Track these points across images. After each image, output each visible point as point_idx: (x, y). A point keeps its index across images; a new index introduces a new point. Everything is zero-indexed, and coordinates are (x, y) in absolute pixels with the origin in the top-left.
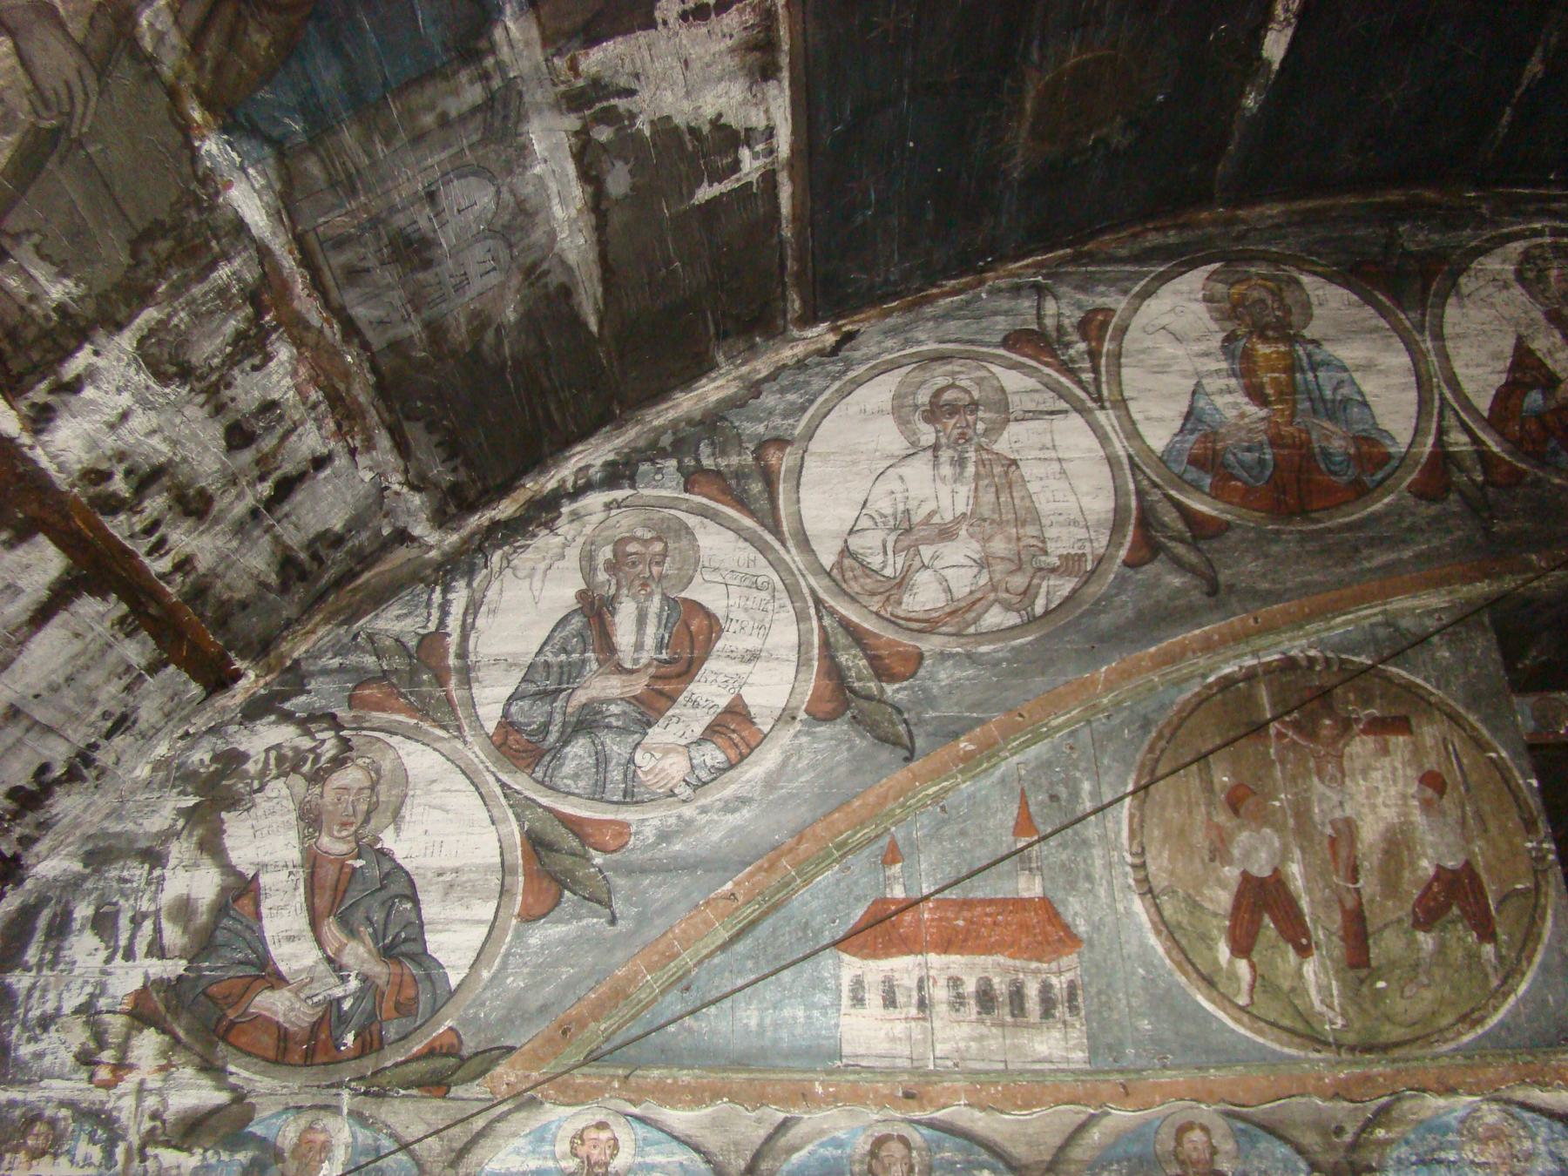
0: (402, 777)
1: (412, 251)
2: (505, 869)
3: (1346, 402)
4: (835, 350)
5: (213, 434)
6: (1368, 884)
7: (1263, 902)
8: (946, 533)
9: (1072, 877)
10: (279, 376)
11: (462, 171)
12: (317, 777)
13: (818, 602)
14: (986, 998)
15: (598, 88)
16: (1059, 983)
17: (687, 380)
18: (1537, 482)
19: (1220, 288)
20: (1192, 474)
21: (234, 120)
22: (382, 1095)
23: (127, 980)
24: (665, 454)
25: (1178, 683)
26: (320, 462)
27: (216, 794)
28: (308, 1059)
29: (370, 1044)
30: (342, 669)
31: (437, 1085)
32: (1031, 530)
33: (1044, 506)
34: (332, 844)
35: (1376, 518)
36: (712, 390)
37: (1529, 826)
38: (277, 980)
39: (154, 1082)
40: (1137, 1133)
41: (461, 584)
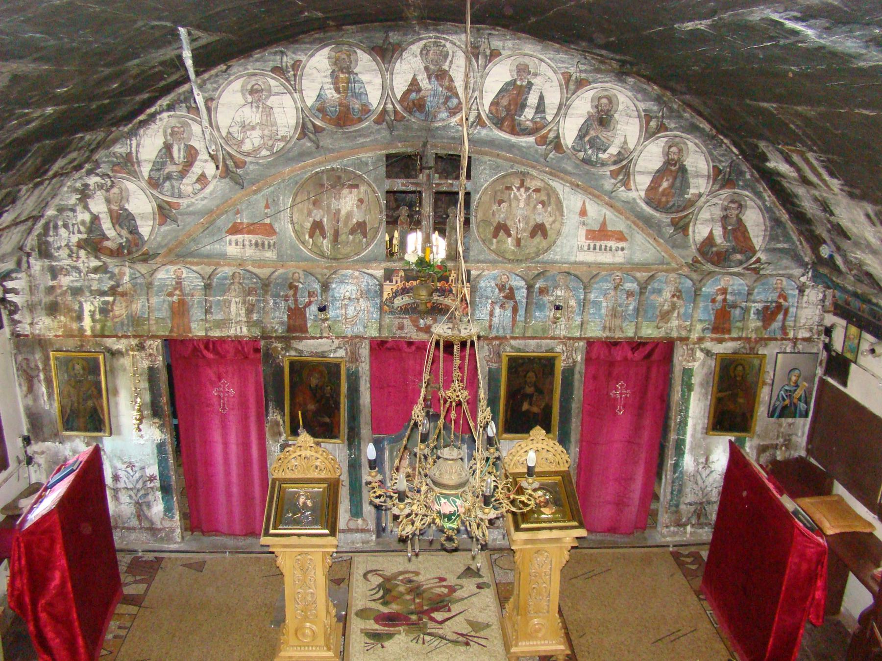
2: (154, 214)
3: (361, 94)
4: (226, 71)
7: (317, 226)
12: (108, 190)
13: (222, 147)
14: (257, 244)
18: (408, 121)
19: (333, 54)
20: (317, 113)
22: (134, 263)
23: (75, 239)
24: (182, 102)
25: (305, 173)
27: (85, 194)
29: (129, 253)
30: (108, 162)
31: (145, 261)
32: (275, 128)
33: (279, 121)
34: (114, 207)
35: (362, 129)
37: (381, 212)
38: (108, 239)
39: (86, 261)
40: (284, 273)
41: (134, 139)
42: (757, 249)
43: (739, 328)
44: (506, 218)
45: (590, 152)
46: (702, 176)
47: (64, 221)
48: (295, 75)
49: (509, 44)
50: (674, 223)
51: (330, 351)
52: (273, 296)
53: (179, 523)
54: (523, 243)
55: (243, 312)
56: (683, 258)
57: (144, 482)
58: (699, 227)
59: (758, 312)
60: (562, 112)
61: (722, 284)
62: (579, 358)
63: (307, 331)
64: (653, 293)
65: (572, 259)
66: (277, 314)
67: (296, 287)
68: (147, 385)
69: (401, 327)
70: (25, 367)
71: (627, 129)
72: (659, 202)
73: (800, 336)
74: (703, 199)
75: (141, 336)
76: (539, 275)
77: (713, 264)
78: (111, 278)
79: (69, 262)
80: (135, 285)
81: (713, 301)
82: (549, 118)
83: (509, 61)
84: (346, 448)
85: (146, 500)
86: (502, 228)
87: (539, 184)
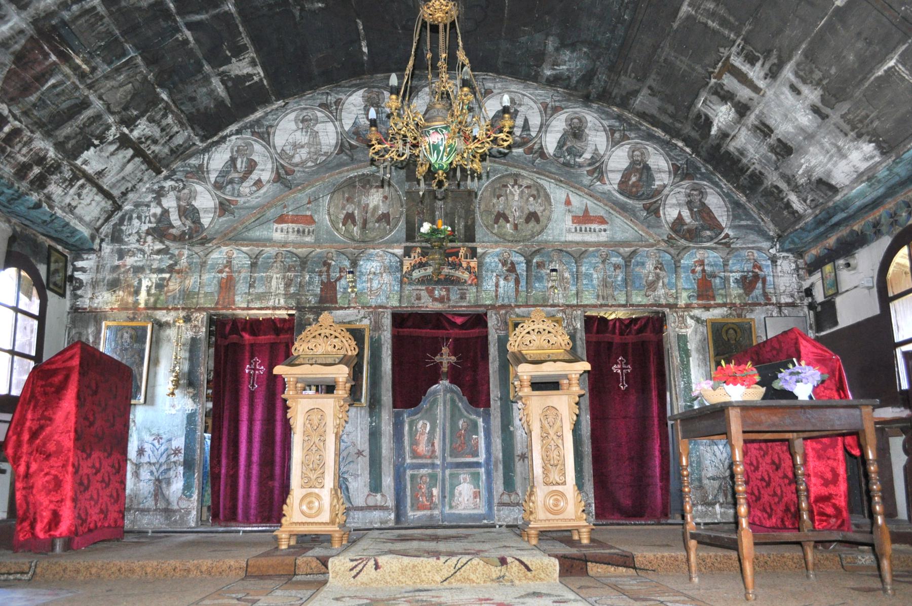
0: (196, 192)
1: (192, 99)
2: (215, 208)
5: (158, 130)
7: (350, 217)
8: (302, 147)
10: (170, 119)
12: (179, 191)
14: (298, 231)
15: (223, 72)
17: (253, 113)
23: (145, 227)
26: (177, 132)
27: (160, 194)
28: (180, 240)
31: (203, 244)
33: (322, 142)
34: (183, 203)
36: (258, 114)
37: (402, 206)
38: (173, 227)
40: (320, 253)
42: (724, 226)
43: (722, 295)
46: (664, 172)
48: (337, 109)
49: (499, 85)
50: (646, 208)
51: (356, 321)
53: (196, 504)
55: (282, 286)
57: (168, 456)
58: (668, 210)
59: (737, 281)
60: (543, 129)
61: (698, 256)
63: (337, 303)
65: (563, 239)
66: (311, 287)
67: (330, 264)
68: (187, 355)
69: (419, 298)
71: (597, 140)
72: (631, 192)
73: (783, 301)
74: (668, 189)
75: (189, 309)
76: (535, 252)
77: (686, 239)
78: (170, 258)
79: (137, 245)
80: (190, 264)
81: (693, 271)
82: (533, 134)
84: (368, 415)
86: (502, 216)
87: (529, 182)
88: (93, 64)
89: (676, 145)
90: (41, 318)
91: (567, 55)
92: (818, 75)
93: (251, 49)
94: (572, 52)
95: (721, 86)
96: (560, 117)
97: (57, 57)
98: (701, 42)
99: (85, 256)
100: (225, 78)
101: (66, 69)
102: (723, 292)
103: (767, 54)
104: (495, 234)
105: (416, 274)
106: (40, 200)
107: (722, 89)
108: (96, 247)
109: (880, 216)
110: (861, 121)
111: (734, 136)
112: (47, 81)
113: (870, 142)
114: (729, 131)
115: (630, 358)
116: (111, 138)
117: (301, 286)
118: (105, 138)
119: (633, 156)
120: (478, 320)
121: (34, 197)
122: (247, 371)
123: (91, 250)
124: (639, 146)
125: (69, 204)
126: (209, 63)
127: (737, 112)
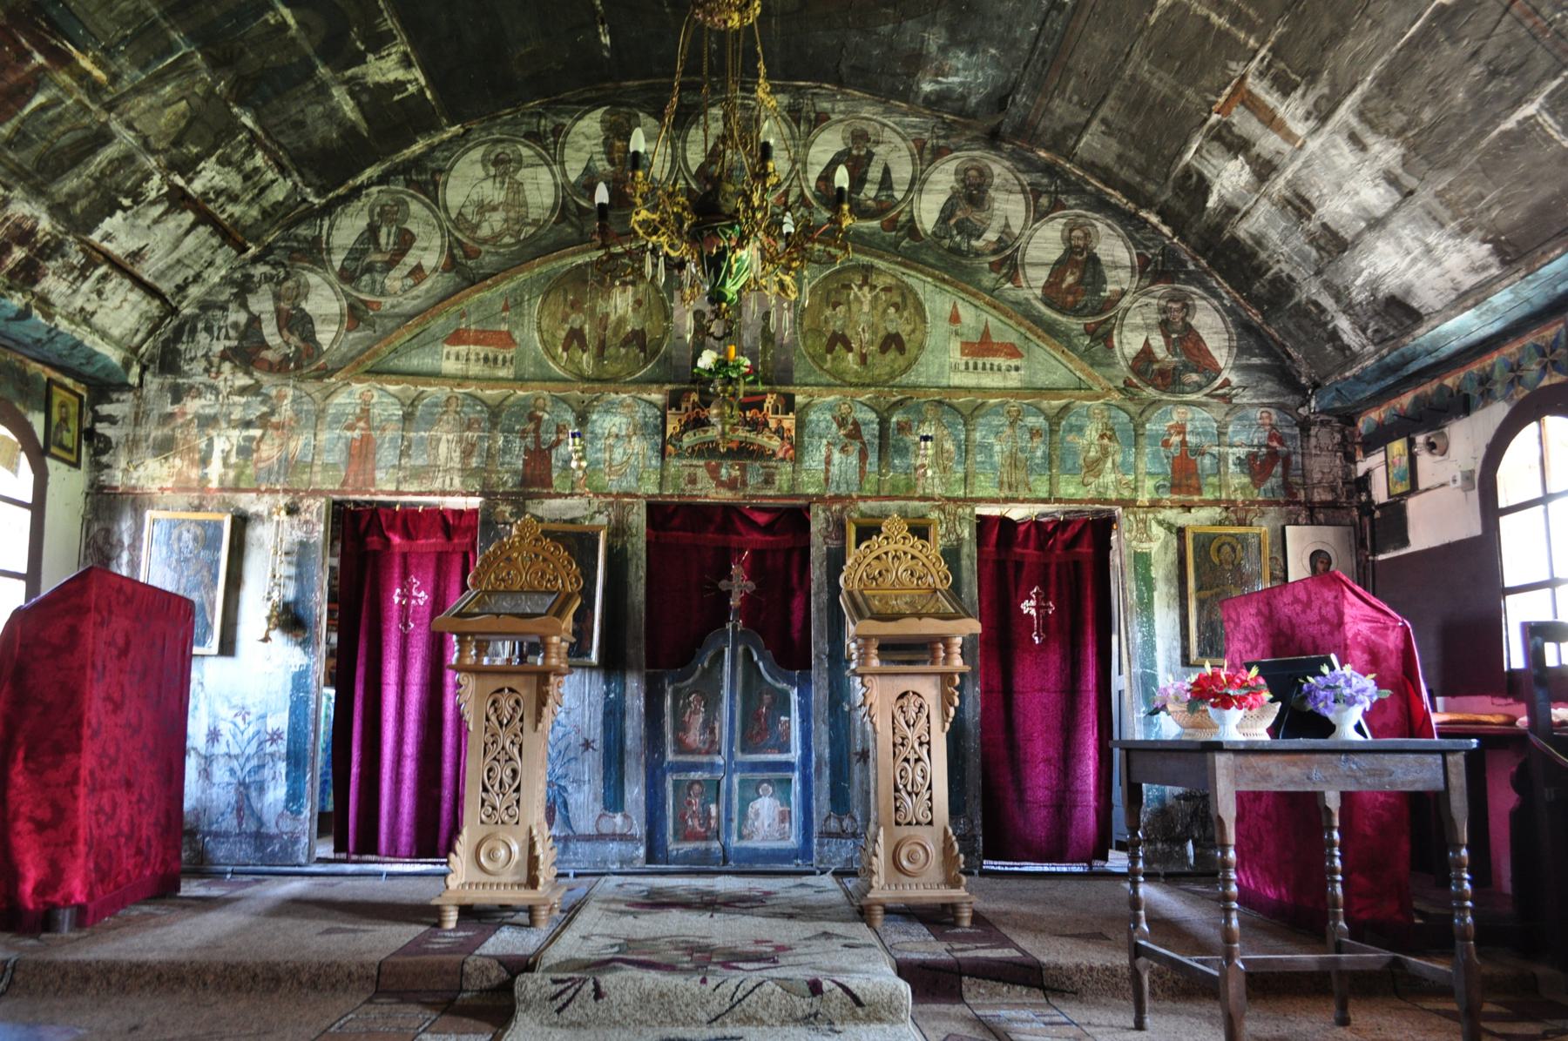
0: (308, 285)
1: (299, 125)
2: (342, 315)
4: (464, 134)
5: (239, 178)
6: (609, 333)
7: (575, 338)
8: (495, 209)
9: (517, 325)
10: (259, 159)
11: (311, 104)
12: (279, 283)
14: (486, 359)
15: (352, 78)
16: (508, 356)
17: (408, 147)
21: (241, 103)
23: (218, 347)
26: (273, 182)
28: (279, 371)
31: (319, 378)
33: (529, 200)
34: (284, 305)
36: (418, 147)
38: (268, 347)
40: (525, 398)
42: (1222, 365)
43: (1212, 485)
44: (844, 326)
45: (958, 239)
47: (207, 322)
50: (1089, 331)
51: (585, 518)
52: (503, 431)
54: (870, 359)
55: (457, 455)
56: (1110, 380)
57: (260, 744)
59: (1240, 462)
60: (916, 187)
62: (966, 534)
63: (550, 485)
64: (1071, 431)
65: (944, 382)
66: (507, 458)
67: (540, 419)
68: (292, 571)
69: (693, 480)
70: (100, 541)
71: (1009, 207)
73: (1317, 498)
75: (296, 492)
76: (895, 404)
77: (1156, 387)
78: (263, 402)
79: (205, 378)
80: (297, 413)
82: (899, 195)
83: (841, 127)
85: (257, 778)
86: (839, 340)
87: (889, 281)
88: (114, 68)
89: (1146, 221)
90: (37, 508)
91: (960, 58)
92: (1399, 119)
93: (402, 37)
94: (971, 54)
95: (1228, 126)
96: (946, 167)
97: (47, 58)
98: (1197, 52)
99: (115, 396)
100: (357, 89)
101: (64, 78)
102: (1214, 480)
103: (1312, 76)
104: (828, 371)
105: (688, 440)
106: (27, 305)
107: (1230, 131)
108: (133, 379)
109: (1493, 366)
110: (1469, 204)
111: (1247, 213)
112: (29, 99)
113: (1484, 241)
114: (1239, 204)
115: (1053, 589)
116: (153, 195)
117: (490, 455)
118: (141, 194)
119: (1069, 239)
120: (793, 519)
121: (17, 301)
122: (396, 599)
123: (124, 387)
124: (1081, 221)
125: (82, 309)
126: (326, 63)
127: (1254, 172)
